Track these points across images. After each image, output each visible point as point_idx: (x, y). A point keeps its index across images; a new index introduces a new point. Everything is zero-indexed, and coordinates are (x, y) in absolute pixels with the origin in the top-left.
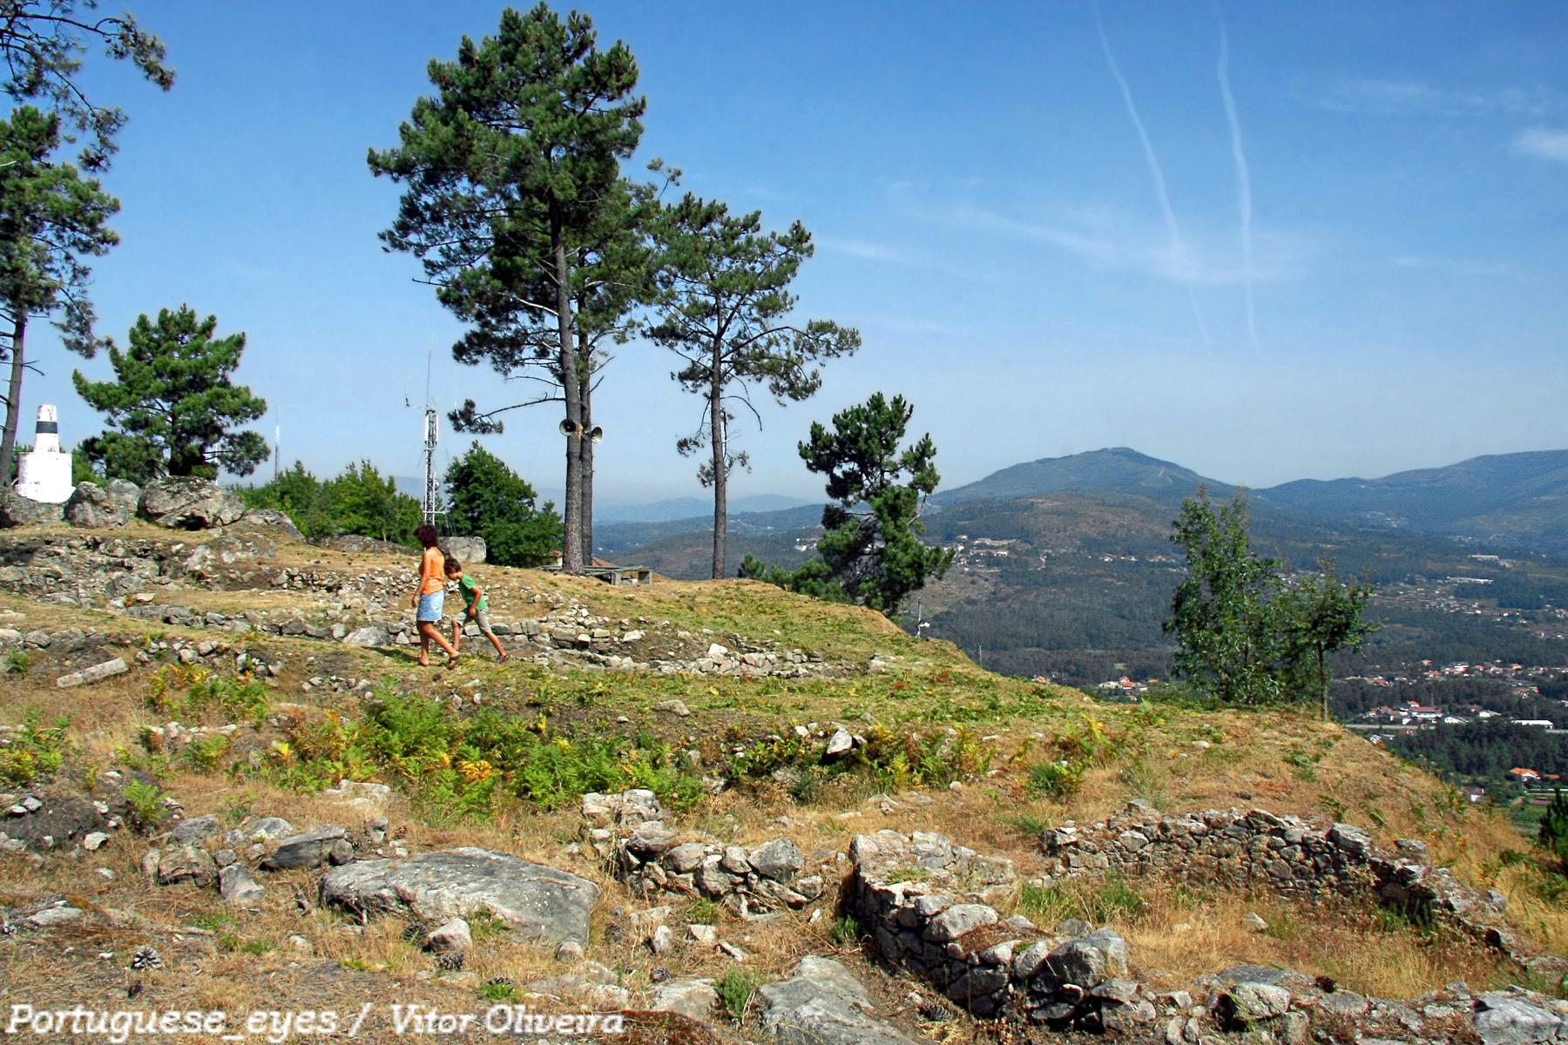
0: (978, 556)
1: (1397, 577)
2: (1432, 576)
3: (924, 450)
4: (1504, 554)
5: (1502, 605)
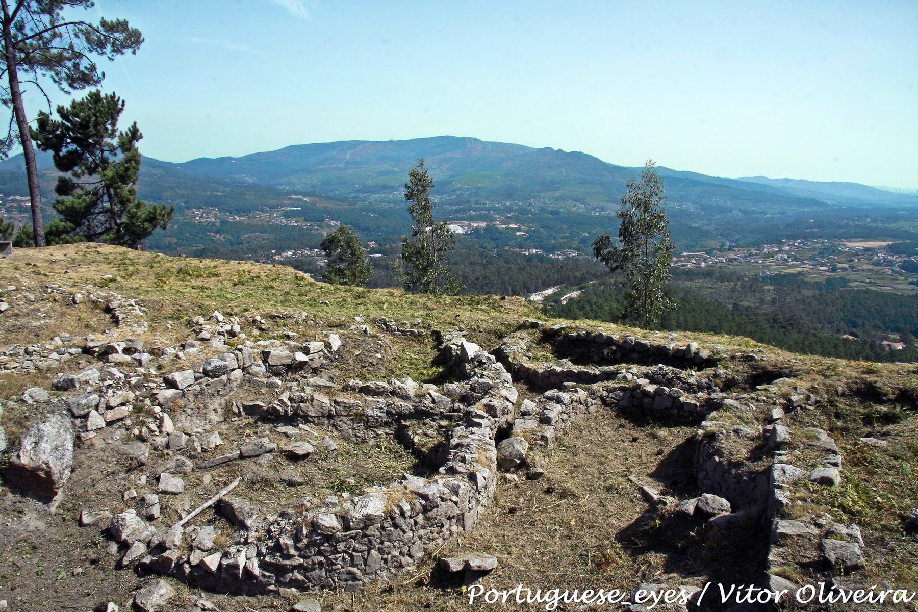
0: (12, 207)
1: (255, 208)
2: (272, 207)
3: (134, 134)
4: (306, 194)
5: (306, 220)
